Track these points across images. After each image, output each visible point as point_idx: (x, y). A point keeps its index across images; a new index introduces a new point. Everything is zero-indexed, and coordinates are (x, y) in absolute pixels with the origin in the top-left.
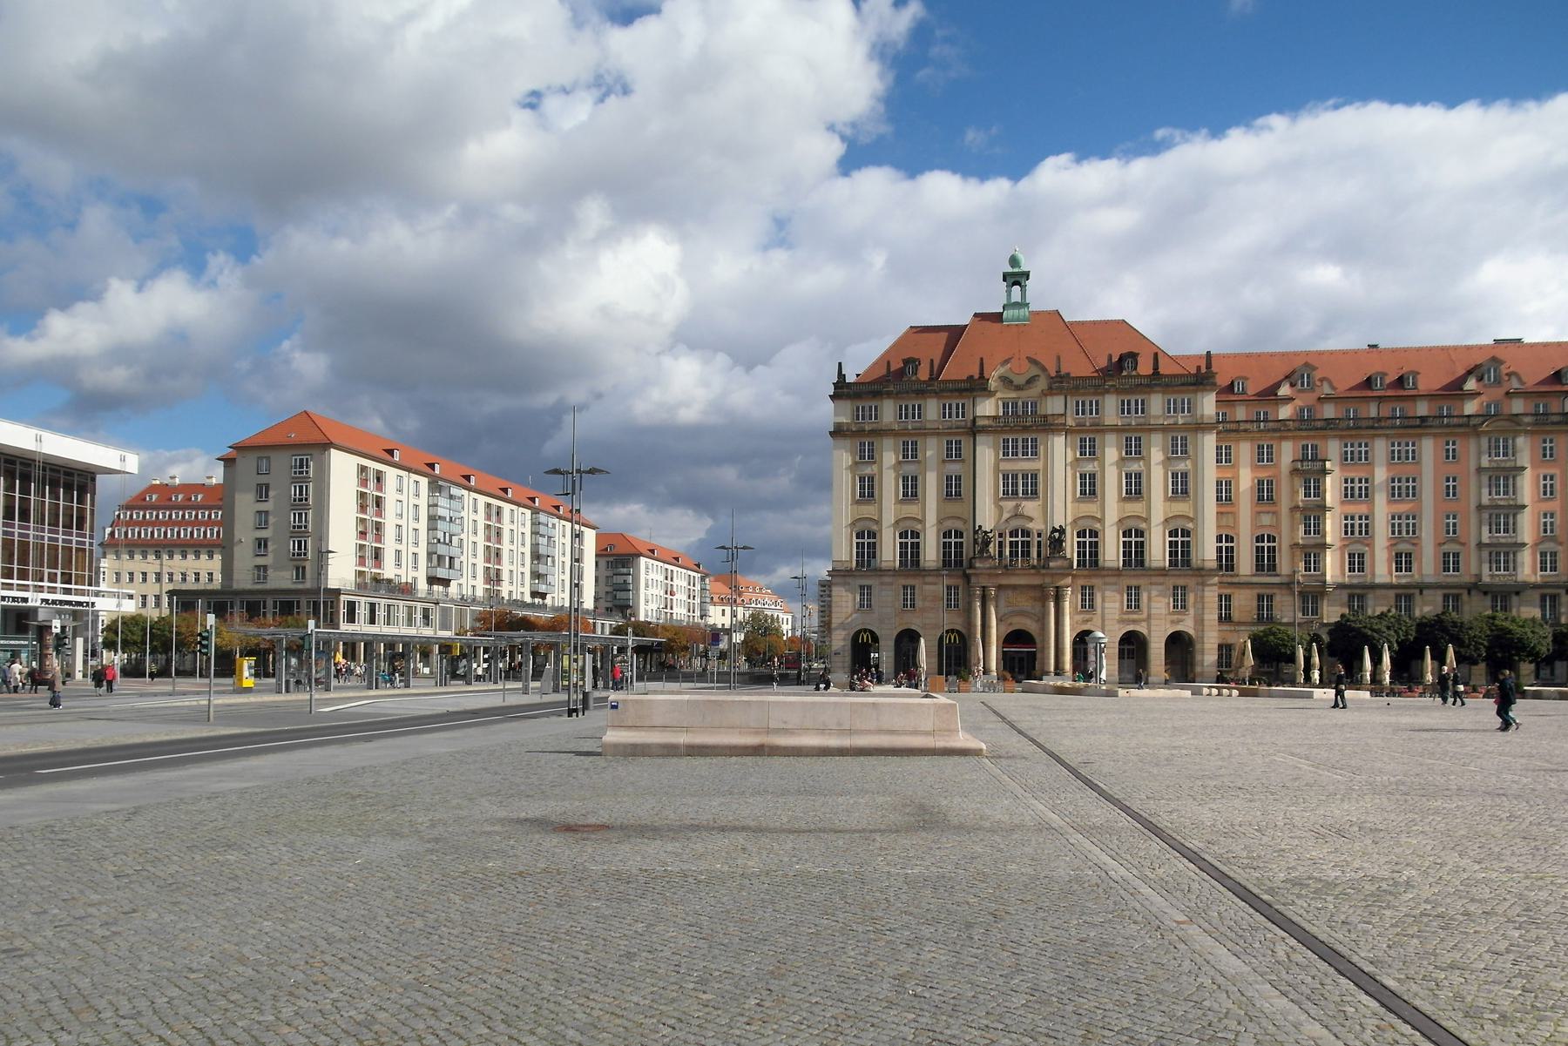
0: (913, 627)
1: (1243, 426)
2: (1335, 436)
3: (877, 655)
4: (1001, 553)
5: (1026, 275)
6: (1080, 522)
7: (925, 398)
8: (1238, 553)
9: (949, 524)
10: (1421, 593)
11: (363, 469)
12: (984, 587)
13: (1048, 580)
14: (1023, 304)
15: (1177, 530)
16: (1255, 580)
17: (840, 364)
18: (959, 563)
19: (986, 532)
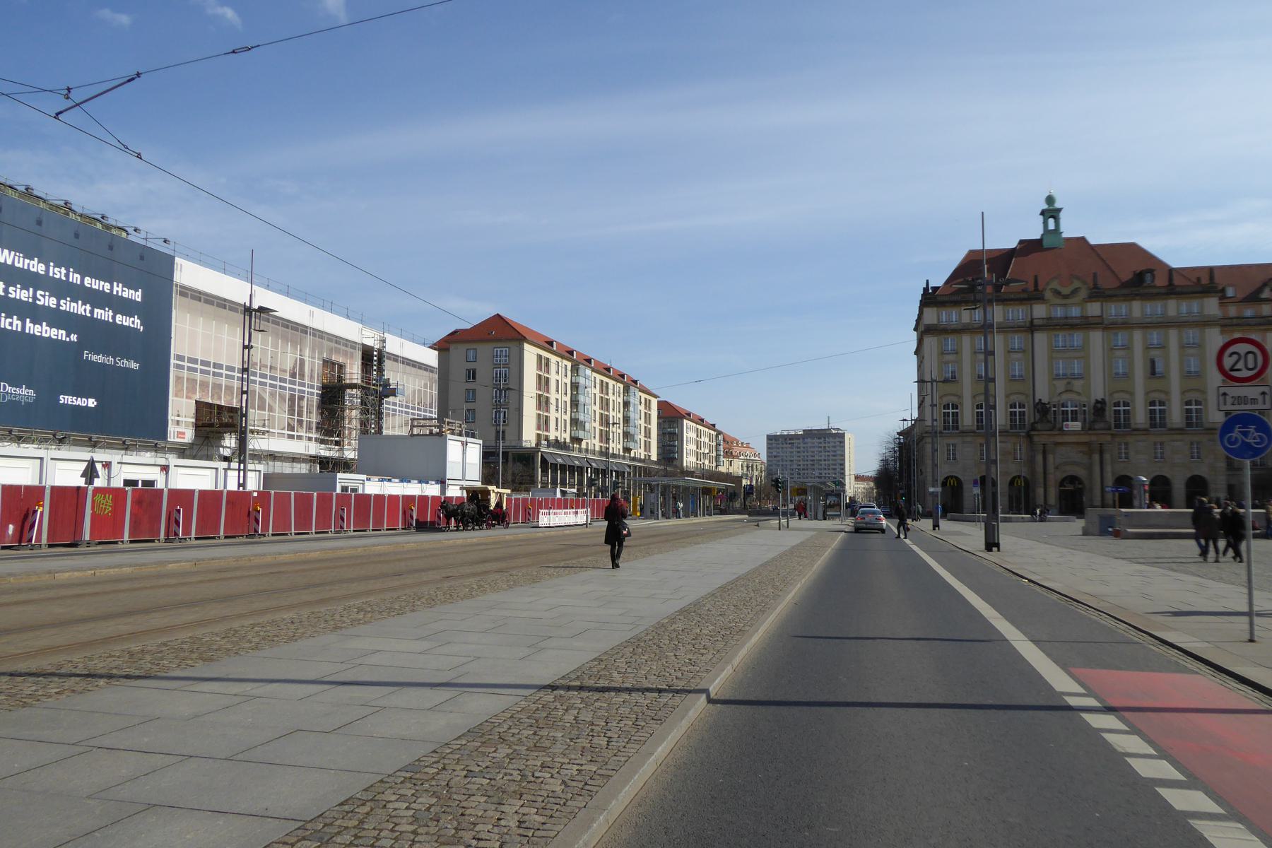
1: (1235, 321)
4: (1055, 418)
5: (1059, 210)
6: (1116, 396)
9: (1015, 398)
11: (540, 357)
12: (1044, 444)
13: (1094, 438)
14: (1057, 230)
15: (1119, 402)
18: (1022, 426)
19: (1044, 404)
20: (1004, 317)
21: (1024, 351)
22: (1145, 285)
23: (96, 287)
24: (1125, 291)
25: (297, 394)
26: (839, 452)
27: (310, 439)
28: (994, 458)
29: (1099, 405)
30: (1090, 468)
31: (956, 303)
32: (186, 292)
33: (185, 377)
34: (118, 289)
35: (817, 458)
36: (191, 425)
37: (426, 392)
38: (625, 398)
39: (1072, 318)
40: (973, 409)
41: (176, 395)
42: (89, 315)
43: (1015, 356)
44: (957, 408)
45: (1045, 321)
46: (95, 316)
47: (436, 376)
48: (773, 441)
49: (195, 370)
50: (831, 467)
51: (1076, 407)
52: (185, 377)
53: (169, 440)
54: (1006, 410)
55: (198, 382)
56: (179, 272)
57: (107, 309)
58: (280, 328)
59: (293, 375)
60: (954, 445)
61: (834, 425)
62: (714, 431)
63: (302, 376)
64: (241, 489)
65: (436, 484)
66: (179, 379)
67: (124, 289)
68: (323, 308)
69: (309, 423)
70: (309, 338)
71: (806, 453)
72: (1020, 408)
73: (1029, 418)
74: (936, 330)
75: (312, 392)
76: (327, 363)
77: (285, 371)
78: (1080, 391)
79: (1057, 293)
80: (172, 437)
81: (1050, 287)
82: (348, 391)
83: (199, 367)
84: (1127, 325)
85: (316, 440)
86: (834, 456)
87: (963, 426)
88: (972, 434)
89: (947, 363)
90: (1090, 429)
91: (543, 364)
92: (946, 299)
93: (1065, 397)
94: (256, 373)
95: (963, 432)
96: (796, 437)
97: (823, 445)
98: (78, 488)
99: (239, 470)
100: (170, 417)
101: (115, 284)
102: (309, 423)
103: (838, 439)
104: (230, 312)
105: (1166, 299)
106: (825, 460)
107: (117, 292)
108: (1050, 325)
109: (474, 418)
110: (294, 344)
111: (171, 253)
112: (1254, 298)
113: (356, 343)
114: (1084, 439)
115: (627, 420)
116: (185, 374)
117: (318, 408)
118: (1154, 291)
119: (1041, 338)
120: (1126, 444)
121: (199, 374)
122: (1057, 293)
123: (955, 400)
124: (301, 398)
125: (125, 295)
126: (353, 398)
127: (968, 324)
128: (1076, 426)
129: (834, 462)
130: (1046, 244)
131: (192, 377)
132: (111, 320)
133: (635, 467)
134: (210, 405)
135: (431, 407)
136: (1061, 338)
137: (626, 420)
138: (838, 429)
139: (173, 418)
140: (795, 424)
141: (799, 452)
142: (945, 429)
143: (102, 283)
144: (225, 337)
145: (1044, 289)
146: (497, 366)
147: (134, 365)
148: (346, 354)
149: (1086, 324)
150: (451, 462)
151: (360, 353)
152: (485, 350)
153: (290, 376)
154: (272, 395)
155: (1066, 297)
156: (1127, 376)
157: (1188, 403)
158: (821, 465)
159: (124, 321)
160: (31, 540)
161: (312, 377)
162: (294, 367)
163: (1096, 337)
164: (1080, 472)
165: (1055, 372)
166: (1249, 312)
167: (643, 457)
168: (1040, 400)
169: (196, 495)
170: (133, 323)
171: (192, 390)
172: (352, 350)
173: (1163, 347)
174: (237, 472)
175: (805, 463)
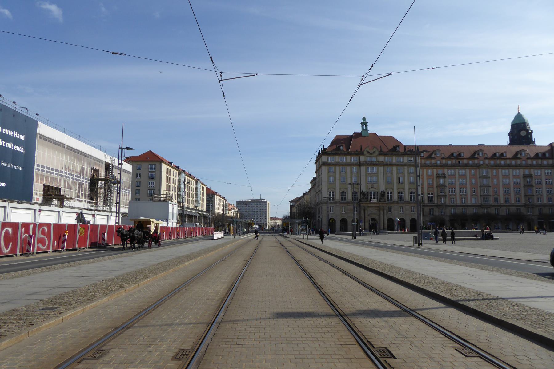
0: (345, 218)
2: (446, 168)
3: (353, 224)
7: (347, 156)
8: (347, 196)
10: (501, 208)
13: (381, 205)
16: (428, 205)
17: (361, 146)
19: (364, 192)
20: (396, 161)
21: (357, 173)
22: (397, 151)
23: (7, 133)
24: (391, 153)
25: (81, 182)
26: (264, 208)
27: (85, 201)
28: (420, 213)
29: (383, 193)
30: (379, 215)
31: (334, 154)
32: (42, 137)
33: (40, 174)
34: (16, 134)
35: (256, 210)
36: (41, 195)
37: (127, 182)
38: (196, 186)
39: (373, 162)
40: (351, 193)
41: (36, 182)
42: (4, 145)
43: (354, 174)
44: (392, 193)
45: (364, 162)
46: (7, 146)
47: (131, 176)
48: (239, 204)
49: (44, 171)
50: (261, 214)
51: (375, 193)
52: (40, 174)
53: (33, 201)
54: (351, 194)
55: (45, 176)
56: (39, 128)
57: (11, 143)
58: (76, 154)
59: (80, 174)
60: (333, 207)
61: (263, 198)
62: (225, 199)
63: (83, 174)
64: (117, 224)
65: (166, 221)
66: (37, 175)
67: (18, 134)
68: (92, 146)
69: (85, 195)
70: (86, 158)
71: (252, 209)
72: (390, 193)
73: (359, 197)
74: (326, 164)
75: (87, 181)
76: (93, 169)
77: (77, 172)
78: (376, 188)
79: (368, 152)
80: (34, 200)
81: (366, 150)
82: (100, 181)
83: (45, 169)
84: (391, 165)
85: (88, 202)
86: (262, 210)
87: (336, 200)
88: (339, 203)
89: (330, 176)
90: (379, 201)
91: (168, 172)
92: (330, 152)
93: (371, 190)
94: (46, 172)
95: (405, 202)
96: (248, 202)
97: (258, 206)
98: (75, 224)
99: (116, 216)
100: (34, 192)
101: (15, 132)
102: (85, 195)
103: (264, 203)
104: (58, 146)
105: (404, 156)
106: (259, 211)
107: (15, 135)
108: (366, 164)
109: (139, 193)
110: (81, 162)
111: (36, 119)
112: (472, 157)
113: (103, 161)
114: (378, 205)
115: (196, 195)
116: (40, 172)
117: (89, 188)
118: (399, 153)
119: (363, 168)
120: (391, 207)
121: (45, 173)
122: (368, 152)
123: (333, 190)
124: (83, 184)
125: (18, 137)
126: (101, 184)
127: (338, 162)
128: (375, 200)
129: (263, 212)
130: (363, 134)
131: (43, 174)
132: (12, 148)
133: (200, 214)
134: (48, 186)
135: (129, 189)
136: (370, 168)
137: (196, 195)
138: (264, 200)
139: (35, 192)
140: (248, 197)
141: (249, 208)
142: (410, 201)
143: (10, 131)
144: (56, 157)
145: (364, 151)
146: (150, 172)
147: (20, 168)
148: (99, 165)
149: (378, 164)
150: (170, 213)
151: (105, 165)
152: (145, 165)
153: (79, 175)
154: (72, 182)
155: (371, 154)
156: (391, 183)
157: (429, 194)
158: (257, 213)
159: (17, 148)
160: (63, 248)
161: (87, 175)
162: (81, 171)
163: (381, 169)
164: (376, 217)
165: (368, 181)
166: (513, 162)
167: (201, 210)
168: (363, 191)
169: (99, 227)
170: (21, 149)
171: (42, 180)
172: (102, 164)
173: (403, 173)
174: (115, 217)
175: (252, 212)
